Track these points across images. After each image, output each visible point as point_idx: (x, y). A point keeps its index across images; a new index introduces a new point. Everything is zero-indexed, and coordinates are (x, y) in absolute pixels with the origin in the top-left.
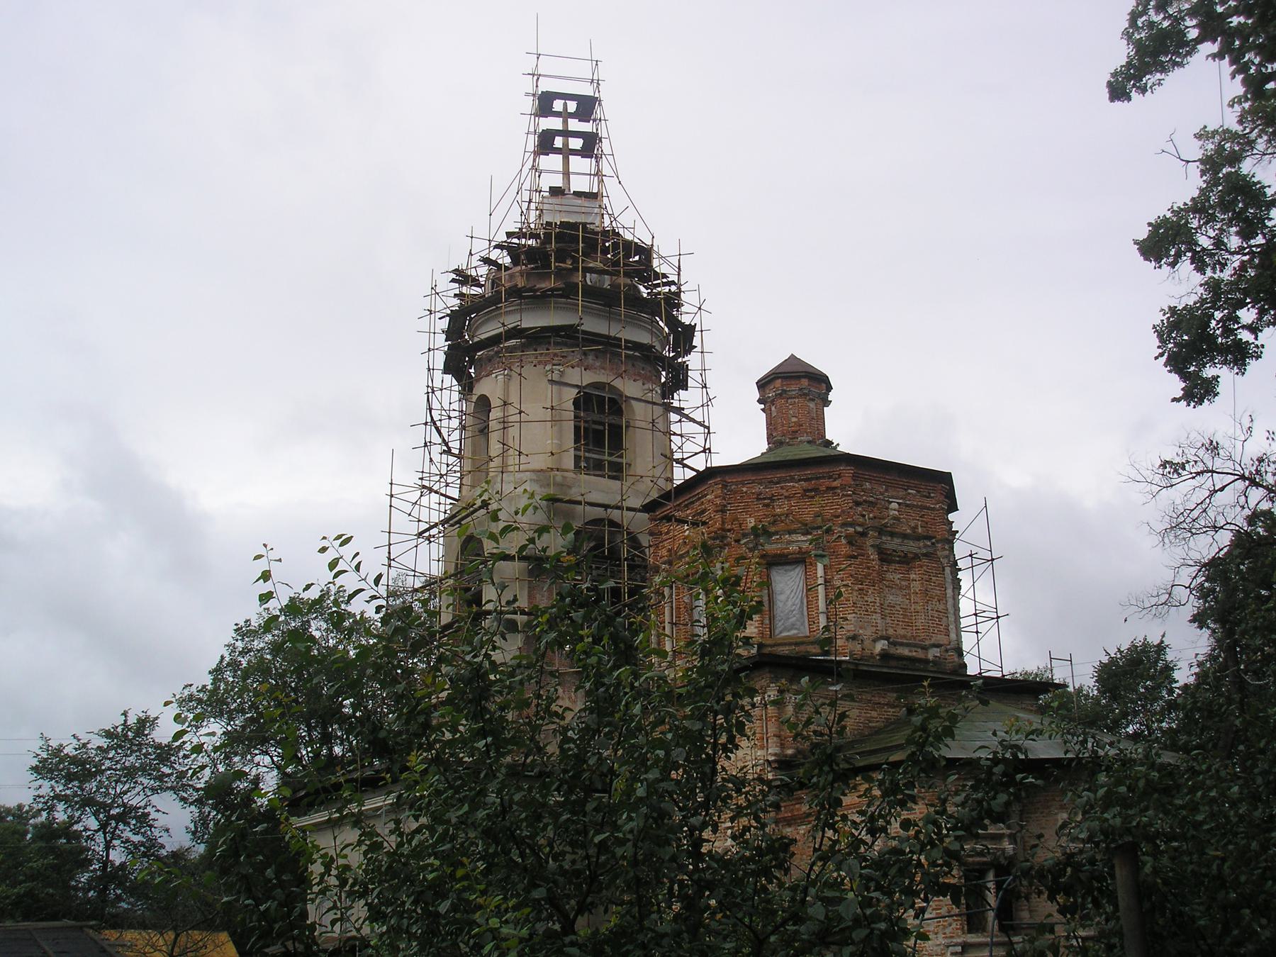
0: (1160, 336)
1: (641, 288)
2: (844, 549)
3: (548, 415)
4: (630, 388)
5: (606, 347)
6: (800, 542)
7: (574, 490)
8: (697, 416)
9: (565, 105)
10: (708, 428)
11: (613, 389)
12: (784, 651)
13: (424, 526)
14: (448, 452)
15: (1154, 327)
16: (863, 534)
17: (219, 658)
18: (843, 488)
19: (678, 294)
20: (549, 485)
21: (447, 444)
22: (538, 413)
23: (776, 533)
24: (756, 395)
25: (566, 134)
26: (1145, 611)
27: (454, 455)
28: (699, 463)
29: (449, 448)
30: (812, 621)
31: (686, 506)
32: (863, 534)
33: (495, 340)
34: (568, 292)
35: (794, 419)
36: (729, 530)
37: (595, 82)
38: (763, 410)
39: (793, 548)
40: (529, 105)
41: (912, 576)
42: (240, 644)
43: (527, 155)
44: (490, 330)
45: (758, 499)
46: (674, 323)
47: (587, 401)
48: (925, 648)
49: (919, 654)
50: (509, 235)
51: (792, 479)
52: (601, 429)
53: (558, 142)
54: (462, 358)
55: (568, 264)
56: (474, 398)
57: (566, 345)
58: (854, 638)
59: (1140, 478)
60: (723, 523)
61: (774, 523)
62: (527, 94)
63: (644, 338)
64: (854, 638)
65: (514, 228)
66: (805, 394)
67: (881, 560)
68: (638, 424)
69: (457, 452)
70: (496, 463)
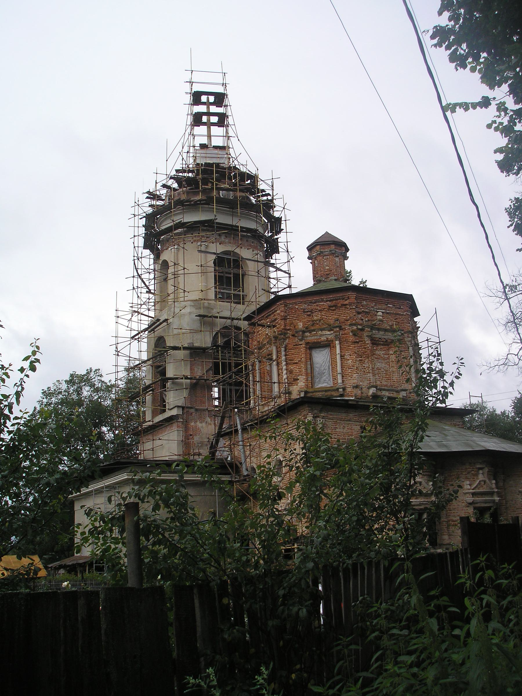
0: (509, 214)
1: (252, 198)
2: (352, 339)
3: (199, 270)
4: (245, 253)
5: (231, 231)
6: (328, 335)
7: (215, 310)
8: (285, 268)
9: (208, 98)
10: (289, 274)
11: (235, 254)
12: (319, 395)
13: (134, 333)
14: (149, 292)
15: (506, 209)
16: (362, 330)
17: (33, 409)
18: (350, 304)
19: (272, 201)
20: (200, 308)
21: (148, 288)
22: (194, 267)
23: (314, 330)
24: (307, 254)
25: (209, 114)
26: (491, 369)
27: (152, 293)
28: (264, 300)
29: (150, 290)
30: (335, 379)
31: (267, 317)
32: (362, 330)
33: (169, 230)
34: (209, 201)
35: (327, 268)
36: (289, 330)
37: (224, 85)
38: (311, 263)
39: (323, 338)
40: (188, 99)
41: (391, 352)
42: (45, 400)
43: (187, 126)
44: (167, 224)
45: (304, 312)
46: (270, 217)
47: (219, 261)
48: (398, 392)
49: (395, 395)
50: (177, 171)
51: (322, 301)
52: (229, 276)
53: (205, 119)
54: (154, 240)
55: (209, 186)
56: (161, 262)
57: (208, 231)
58: (357, 387)
59: (492, 295)
60: (285, 326)
61: (312, 325)
62: (187, 93)
63: (252, 225)
64: (357, 387)
65: (179, 167)
66: (333, 254)
67: (373, 344)
68: (250, 273)
69: (153, 291)
70: (172, 296)
